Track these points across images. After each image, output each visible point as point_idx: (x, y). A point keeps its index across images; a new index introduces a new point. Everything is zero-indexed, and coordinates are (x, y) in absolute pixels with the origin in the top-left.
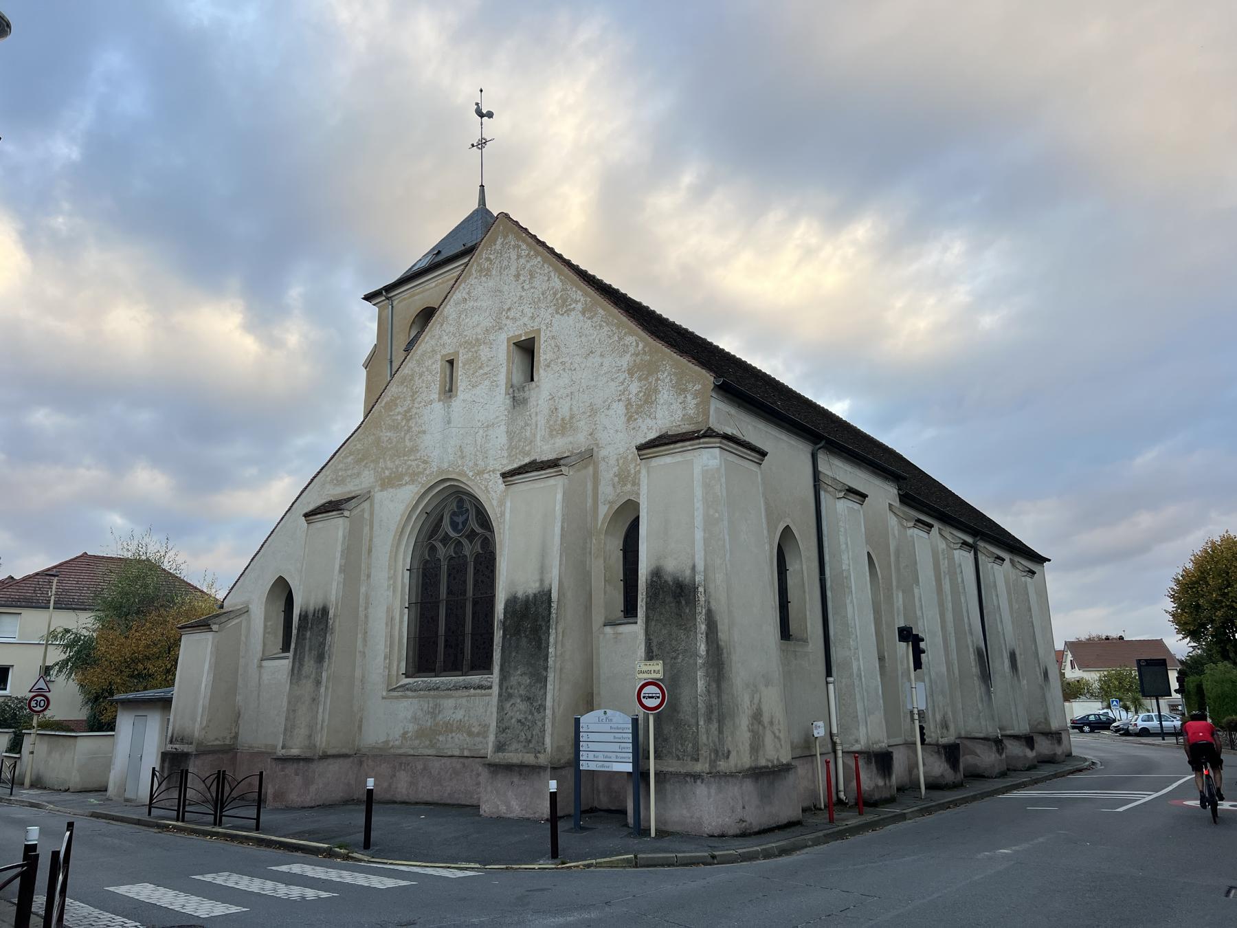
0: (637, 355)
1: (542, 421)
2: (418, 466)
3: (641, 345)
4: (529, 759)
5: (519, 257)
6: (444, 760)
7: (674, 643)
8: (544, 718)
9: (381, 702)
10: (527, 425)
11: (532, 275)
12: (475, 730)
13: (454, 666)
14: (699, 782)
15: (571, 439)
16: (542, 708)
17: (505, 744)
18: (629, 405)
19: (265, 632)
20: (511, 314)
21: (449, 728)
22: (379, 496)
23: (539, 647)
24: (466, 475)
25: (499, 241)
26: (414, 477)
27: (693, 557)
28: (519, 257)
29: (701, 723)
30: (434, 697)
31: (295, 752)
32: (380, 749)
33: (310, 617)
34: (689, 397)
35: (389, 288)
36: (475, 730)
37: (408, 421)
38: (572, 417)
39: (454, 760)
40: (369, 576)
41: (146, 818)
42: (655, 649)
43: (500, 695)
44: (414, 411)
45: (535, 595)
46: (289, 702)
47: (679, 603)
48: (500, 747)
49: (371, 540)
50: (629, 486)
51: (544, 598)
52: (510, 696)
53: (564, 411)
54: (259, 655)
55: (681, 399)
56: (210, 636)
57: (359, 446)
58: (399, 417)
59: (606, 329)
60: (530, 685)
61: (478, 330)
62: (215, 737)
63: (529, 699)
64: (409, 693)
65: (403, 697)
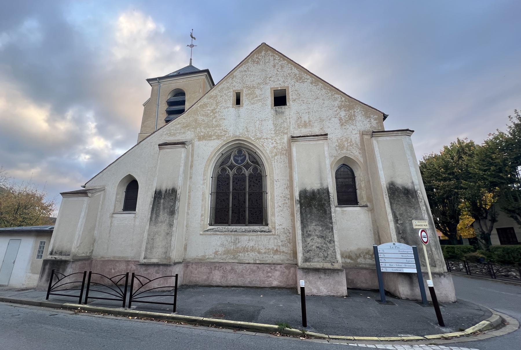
0: (342, 102)
1: (293, 122)
2: (221, 133)
3: (343, 99)
4: (328, 265)
5: (274, 59)
6: (244, 265)
7: (409, 214)
8: (334, 246)
9: (198, 237)
10: (284, 122)
11: (282, 67)
12: (263, 251)
13: (239, 220)
14: (442, 277)
15: (309, 130)
16: (332, 241)
17: (310, 258)
18: (340, 119)
19: (116, 201)
20: (272, 79)
21: (245, 250)
22: (197, 143)
23: (325, 212)
24: (250, 139)
25: (263, 53)
26: (218, 137)
27: (411, 179)
28: (274, 59)
29: (434, 249)
30: (234, 235)
31: (155, 261)
32: (200, 259)
33: (163, 192)
34: (372, 120)
35: (160, 78)
36: (263, 251)
37: (214, 113)
38: (310, 121)
39: (251, 265)
40: (191, 178)
41: (44, 300)
42: (398, 216)
43: (303, 235)
44: (217, 110)
45: (318, 190)
46: (149, 235)
47: (408, 197)
48: (306, 260)
49: (192, 162)
50: (345, 151)
51: (55, 219)
52: (309, 235)
53: (305, 118)
54: (112, 211)
55: (368, 120)
56: (86, 199)
57: (184, 121)
58: (209, 112)
59: (324, 91)
60: (322, 230)
61: (254, 83)
62: (82, 252)
63: (323, 237)
64: (218, 233)
65: (213, 234)
